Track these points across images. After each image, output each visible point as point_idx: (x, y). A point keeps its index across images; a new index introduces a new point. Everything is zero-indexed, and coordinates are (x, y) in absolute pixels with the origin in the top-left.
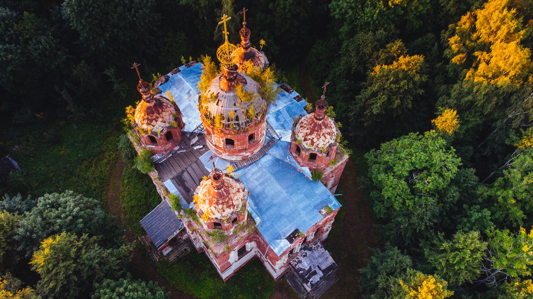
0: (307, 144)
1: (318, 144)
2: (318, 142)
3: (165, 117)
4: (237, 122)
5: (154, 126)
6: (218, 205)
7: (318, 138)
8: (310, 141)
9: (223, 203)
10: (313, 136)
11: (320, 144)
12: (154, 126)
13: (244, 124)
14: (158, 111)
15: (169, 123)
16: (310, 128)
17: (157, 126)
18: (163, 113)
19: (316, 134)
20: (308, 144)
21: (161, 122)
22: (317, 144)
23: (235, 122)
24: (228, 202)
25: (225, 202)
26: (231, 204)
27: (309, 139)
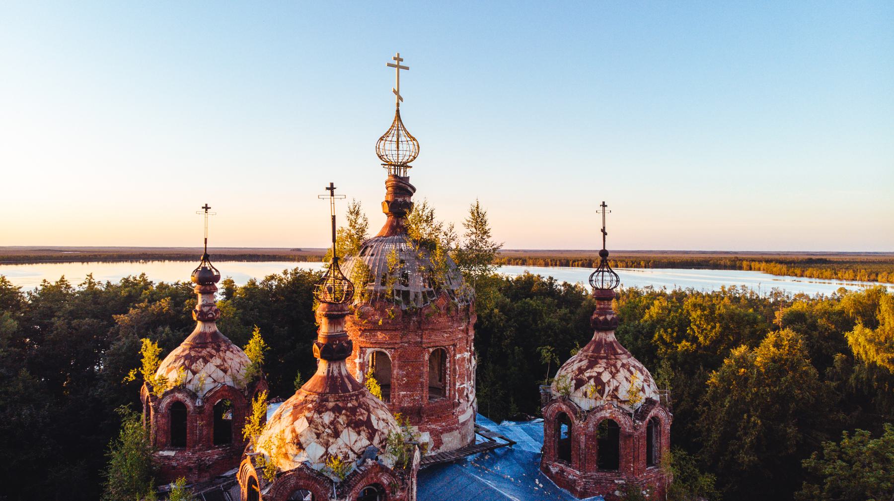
0: (585, 394)
1: (616, 389)
2: (614, 383)
3: (229, 362)
4: (404, 288)
5: (194, 373)
6: (320, 413)
7: (611, 373)
8: (592, 382)
9: (337, 410)
10: (598, 369)
11: (620, 390)
12: (194, 373)
13: (421, 297)
14: (219, 346)
15: (234, 379)
16: (587, 356)
17: (203, 374)
18: (227, 352)
19: (604, 365)
20: (589, 393)
21: (217, 366)
22: (612, 388)
23: (398, 288)
24: (353, 410)
25: (344, 408)
26: (364, 418)
27: (590, 378)
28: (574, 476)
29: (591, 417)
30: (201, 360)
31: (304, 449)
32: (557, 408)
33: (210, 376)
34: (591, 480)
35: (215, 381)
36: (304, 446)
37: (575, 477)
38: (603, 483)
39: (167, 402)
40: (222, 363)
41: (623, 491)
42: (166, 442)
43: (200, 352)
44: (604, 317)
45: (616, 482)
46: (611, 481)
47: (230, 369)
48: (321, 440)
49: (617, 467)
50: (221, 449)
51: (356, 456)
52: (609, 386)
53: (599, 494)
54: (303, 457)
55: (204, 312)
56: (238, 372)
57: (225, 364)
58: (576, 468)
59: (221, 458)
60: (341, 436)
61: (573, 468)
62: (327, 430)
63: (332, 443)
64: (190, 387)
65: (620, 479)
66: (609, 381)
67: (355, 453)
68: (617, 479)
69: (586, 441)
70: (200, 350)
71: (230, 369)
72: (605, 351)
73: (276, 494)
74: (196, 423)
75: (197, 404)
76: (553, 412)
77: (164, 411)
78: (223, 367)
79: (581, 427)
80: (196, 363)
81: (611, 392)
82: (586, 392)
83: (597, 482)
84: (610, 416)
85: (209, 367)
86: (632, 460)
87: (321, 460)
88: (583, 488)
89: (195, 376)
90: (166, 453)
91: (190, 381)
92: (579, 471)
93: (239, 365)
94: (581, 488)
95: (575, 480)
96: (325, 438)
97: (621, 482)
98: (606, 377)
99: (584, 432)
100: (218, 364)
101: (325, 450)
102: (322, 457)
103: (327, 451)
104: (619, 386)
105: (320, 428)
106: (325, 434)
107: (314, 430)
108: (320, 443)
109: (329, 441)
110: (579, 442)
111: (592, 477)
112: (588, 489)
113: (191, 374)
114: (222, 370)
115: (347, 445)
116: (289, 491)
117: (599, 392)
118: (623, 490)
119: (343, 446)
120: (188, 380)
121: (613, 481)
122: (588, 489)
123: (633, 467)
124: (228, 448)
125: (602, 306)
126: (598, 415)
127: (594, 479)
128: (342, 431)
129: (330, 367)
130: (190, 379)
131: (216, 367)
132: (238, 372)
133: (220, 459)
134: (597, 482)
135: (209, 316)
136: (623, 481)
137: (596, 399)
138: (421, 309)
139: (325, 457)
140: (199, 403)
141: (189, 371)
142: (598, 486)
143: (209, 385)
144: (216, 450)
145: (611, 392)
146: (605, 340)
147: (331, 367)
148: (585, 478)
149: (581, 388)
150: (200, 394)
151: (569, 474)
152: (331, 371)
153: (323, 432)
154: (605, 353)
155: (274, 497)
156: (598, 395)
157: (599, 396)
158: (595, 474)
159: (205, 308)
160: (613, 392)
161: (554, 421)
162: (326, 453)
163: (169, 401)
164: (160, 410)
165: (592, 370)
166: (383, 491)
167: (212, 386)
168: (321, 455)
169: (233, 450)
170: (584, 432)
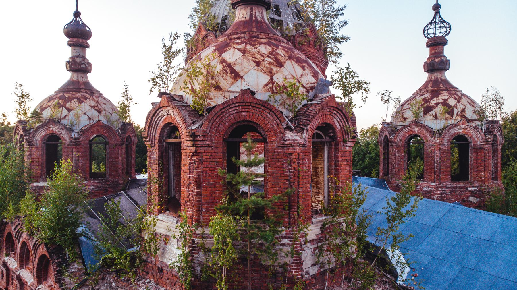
1: (463, 110)
2: (460, 107)
11: (467, 111)
12: (69, 110)
21: (92, 107)
22: (459, 110)
27: (437, 104)
28: (428, 187)
29: (446, 133)
30: (75, 100)
31: (242, 78)
32: (408, 133)
33: (85, 114)
34: (446, 189)
35: (90, 119)
36: (241, 74)
37: (430, 189)
38: (458, 191)
39: (41, 135)
40: (96, 105)
41: (476, 197)
42: (41, 173)
43: (74, 95)
44: (439, 59)
45: (470, 189)
46: (465, 188)
47: (104, 111)
48: (262, 68)
49: (467, 179)
50: (96, 182)
51: (305, 90)
52: (457, 109)
53: (455, 200)
54: (238, 87)
55: (77, 62)
56: (111, 115)
57: (99, 106)
58: (431, 181)
59: (97, 189)
60: (285, 66)
61: (426, 182)
62: (267, 59)
63: (277, 72)
64: (65, 122)
65: (472, 187)
66: (456, 105)
67: (303, 86)
68: (470, 187)
69: (440, 155)
70: (74, 93)
71: (104, 111)
72: (443, 85)
73: (211, 128)
74: (72, 154)
75: (73, 136)
76: (403, 136)
77: (38, 144)
78: (97, 108)
79: (436, 143)
80: (71, 102)
81: (459, 113)
82: (436, 115)
83: (453, 191)
84: (462, 132)
85: (83, 106)
86: (483, 169)
87: (266, 88)
88: (440, 196)
89: (70, 113)
90: (41, 184)
91: (65, 117)
92: (434, 182)
93: (112, 110)
94: (437, 197)
95: (430, 191)
96: (267, 66)
97: (473, 189)
98: (452, 102)
99: (439, 147)
100: (93, 105)
101: (270, 78)
102: (267, 85)
103: (272, 79)
104: (465, 108)
105: (258, 57)
106: (266, 62)
107: (251, 58)
108: (262, 70)
109: (272, 69)
110: (433, 157)
111: (448, 186)
112: (445, 197)
113: (66, 110)
114: (96, 110)
115: (293, 77)
116: (227, 124)
117: (449, 113)
118: (477, 196)
119: (289, 76)
120: (63, 116)
121: (467, 189)
122: (445, 197)
123: (484, 176)
124: (104, 181)
125: (437, 51)
126: (453, 131)
127: (449, 188)
128: (285, 62)
129: (252, 11)
130: (65, 114)
131: (91, 107)
132: (111, 115)
133: (95, 189)
134: (453, 191)
135: (82, 66)
136: (476, 188)
137: (446, 119)
138: (294, 36)
139: (271, 85)
140: (75, 135)
141: (64, 108)
142: (453, 194)
143: (84, 122)
144: (92, 182)
145: (459, 113)
146: (441, 79)
147: (254, 11)
148: (441, 187)
149: (430, 113)
150: (76, 129)
151: (423, 187)
152: (254, 15)
153: (263, 61)
154: (444, 86)
155: (208, 132)
156: (448, 116)
157: (450, 117)
158: (450, 184)
159: (78, 58)
160: (461, 113)
161: (404, 145)
162: (271, 81)
163: (43, 134)
164: (35, 142)
165: (438, 99)
166: (334, 138)
167: (87, 122)
168: (265, 83)
169: (108, 183)
170: (439, 147)
